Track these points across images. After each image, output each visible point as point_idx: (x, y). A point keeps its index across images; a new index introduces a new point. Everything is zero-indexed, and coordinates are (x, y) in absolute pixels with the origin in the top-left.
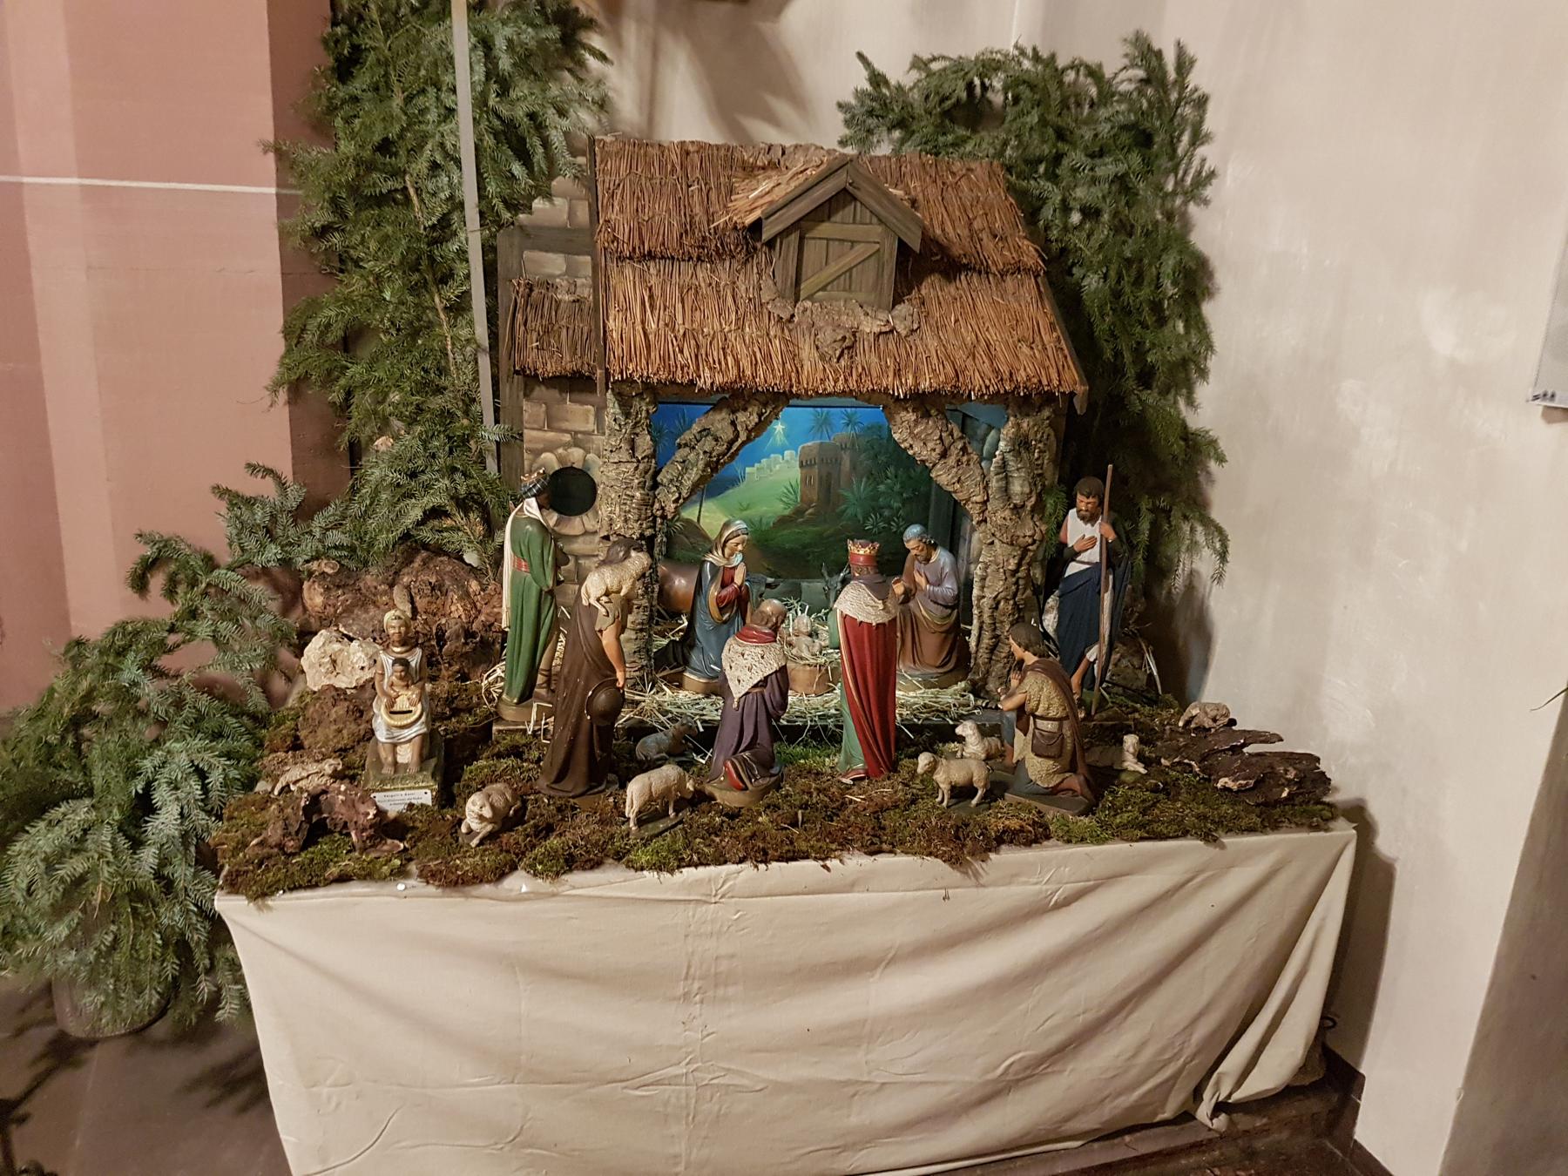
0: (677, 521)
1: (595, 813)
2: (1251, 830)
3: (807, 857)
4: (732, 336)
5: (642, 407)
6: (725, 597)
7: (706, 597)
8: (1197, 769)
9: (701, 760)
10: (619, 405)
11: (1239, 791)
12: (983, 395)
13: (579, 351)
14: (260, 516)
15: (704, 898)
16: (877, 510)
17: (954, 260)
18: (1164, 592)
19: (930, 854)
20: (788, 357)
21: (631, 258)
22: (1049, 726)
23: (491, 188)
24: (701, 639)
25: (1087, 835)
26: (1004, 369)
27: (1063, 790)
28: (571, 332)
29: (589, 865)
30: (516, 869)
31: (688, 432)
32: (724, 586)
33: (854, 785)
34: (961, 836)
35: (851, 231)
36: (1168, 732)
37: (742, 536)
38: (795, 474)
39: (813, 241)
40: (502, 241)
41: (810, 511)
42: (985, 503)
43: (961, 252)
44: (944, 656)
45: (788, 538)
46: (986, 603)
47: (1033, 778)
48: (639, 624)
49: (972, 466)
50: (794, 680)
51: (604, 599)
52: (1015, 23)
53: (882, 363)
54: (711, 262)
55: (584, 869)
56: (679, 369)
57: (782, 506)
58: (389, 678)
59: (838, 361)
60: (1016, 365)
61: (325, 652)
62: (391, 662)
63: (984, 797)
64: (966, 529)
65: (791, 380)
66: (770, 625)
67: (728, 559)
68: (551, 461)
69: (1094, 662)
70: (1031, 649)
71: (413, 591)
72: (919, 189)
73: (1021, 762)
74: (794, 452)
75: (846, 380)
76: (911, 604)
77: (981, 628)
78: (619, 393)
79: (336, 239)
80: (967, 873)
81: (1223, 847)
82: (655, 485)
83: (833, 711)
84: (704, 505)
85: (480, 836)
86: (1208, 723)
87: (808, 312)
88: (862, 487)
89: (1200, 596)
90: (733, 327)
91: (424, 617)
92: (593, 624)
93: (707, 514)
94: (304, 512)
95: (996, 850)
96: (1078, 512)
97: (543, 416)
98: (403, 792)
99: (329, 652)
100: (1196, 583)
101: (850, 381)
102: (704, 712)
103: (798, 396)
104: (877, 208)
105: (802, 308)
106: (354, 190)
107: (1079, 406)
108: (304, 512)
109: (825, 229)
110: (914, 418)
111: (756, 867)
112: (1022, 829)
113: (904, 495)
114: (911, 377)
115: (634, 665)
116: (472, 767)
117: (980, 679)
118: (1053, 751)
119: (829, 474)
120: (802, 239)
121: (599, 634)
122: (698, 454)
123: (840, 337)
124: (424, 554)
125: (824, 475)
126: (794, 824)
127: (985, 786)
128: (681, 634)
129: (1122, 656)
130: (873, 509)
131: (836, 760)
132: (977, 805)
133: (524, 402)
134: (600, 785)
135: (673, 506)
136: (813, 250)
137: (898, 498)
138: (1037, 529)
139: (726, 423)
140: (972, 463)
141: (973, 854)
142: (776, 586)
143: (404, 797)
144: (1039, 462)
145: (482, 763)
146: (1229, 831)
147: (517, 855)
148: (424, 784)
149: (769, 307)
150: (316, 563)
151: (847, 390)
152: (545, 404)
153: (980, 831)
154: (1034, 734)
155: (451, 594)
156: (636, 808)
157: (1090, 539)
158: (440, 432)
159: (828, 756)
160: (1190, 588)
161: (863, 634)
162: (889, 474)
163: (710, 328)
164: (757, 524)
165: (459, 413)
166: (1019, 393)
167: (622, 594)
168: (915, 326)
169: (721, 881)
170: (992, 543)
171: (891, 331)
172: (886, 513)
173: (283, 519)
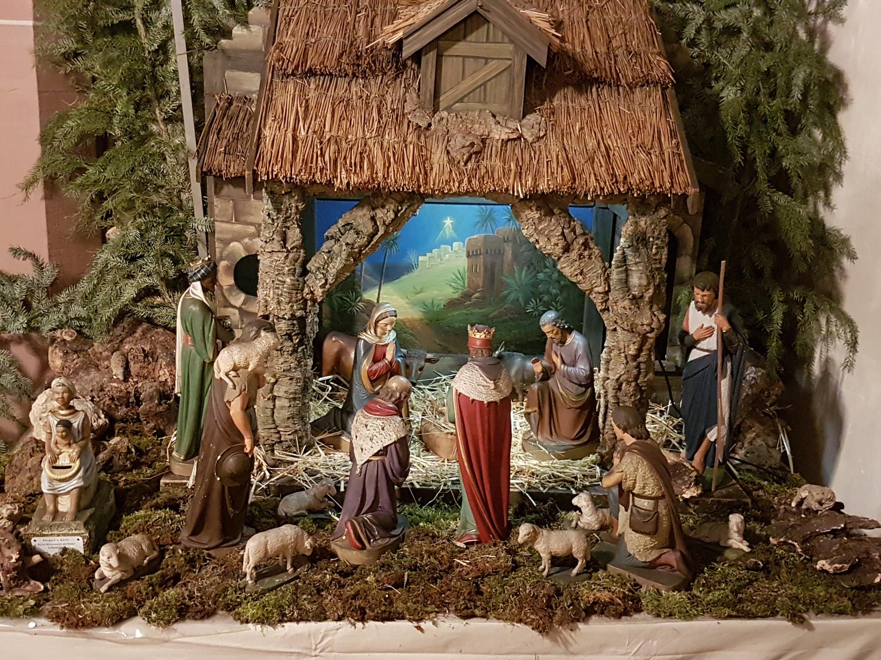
0: (359, 302)
1: (222, 565)
2: (841, 613)
3: (403, 618)
6: (376, 371)
7: (360, 373)
8: (800, 550)
10: (272, 202)
11: (835, 574)
14: (18, 291)
15: (304, 651)
17: (586, 74)
19: (520, 621)
21: (293, 74)
22: (645, 504)
23: (196, 18)
25: (676, 610)
27: (662, 565)
30: (136, 615)
31: (335, 226)
32: (375, 361)
35: (484, 49)
36: (782, 511)
37: (389, 318)
38: (463, 263)
39: (451, 58)
40: (208, 62)
41: (477, 295)
42: (607, 293)
43: (593, 67)
44: (578, 430)
47: (632, 553)
48: (292, 393)
50: (439, 447)
51: (232, 373)
54: (364, 77)
56: (319, 170)
61: (46, 408)
62: (56, 423)
66: (393, 399)
67: (380, 338)
70: (629, 431)
71: (130, 357)
72: (566, 12)
73: (621, 536)
74: (462, 243)
76: (550, 381)
77: (606, 407)
79: (79, 63)
80: (556, 641)
81: (811, 628)
82: (305, 272)
84: (382, 288)
85: (110, 583)
86: (815, 506)
87: (444, 121)
89: (834, 382)
92: (223, 395)
93: (385, 296)
94: (54, 288)
95: (585, 620)
96: (697, 302)
97: (231, 211)
98: (59, 538)
99: (49, 408)
103: (428, 196)
104: (507, 29)
105: (438, 118)
106: (92, 22)
108: (54, 288)
109: (461, 48)
110: (537, 216)
111: (354, 625)
112: (612, 602)
114: (530, 179)
115: (287, 429)
117: (607, 453)
118: (650, 528)
119: (493, 265)
120: (439, 57)
122: (341, 245)
123: (468, 143)
124: (145, 325)
125: (489, 267)
126: (398, 585)
127: (585, 557)
129: (758, 436)
130: (533, 293)
132: (578, 574)
133: (215, 199)
134: (235, 539)
135: (321, 290)
136: (449, 66)
137: (556, 285)
138: (655, 319)
140: (593, 257)
141: (561, 624)
143: (60, 542)
144: (657, 257)
145: (142, 512)
146: (820, 612)
148: (77, 532)
149: (409, 117)
150: (59, 331)
152: (233, 200)
153: (570, 601)
155: (160, 360)
156: (252, 564)
158: (159, 224)
160: (826, 373)
161: (475, 410)
162: (547, 264)
163: (356, 133)
164: (429, 305)
165: (175, 208)
167: (250, 370)
168: (542, 134)
169: (320, 636)
170: (615, 330)
171: (519, 138)
173: (39, 293)
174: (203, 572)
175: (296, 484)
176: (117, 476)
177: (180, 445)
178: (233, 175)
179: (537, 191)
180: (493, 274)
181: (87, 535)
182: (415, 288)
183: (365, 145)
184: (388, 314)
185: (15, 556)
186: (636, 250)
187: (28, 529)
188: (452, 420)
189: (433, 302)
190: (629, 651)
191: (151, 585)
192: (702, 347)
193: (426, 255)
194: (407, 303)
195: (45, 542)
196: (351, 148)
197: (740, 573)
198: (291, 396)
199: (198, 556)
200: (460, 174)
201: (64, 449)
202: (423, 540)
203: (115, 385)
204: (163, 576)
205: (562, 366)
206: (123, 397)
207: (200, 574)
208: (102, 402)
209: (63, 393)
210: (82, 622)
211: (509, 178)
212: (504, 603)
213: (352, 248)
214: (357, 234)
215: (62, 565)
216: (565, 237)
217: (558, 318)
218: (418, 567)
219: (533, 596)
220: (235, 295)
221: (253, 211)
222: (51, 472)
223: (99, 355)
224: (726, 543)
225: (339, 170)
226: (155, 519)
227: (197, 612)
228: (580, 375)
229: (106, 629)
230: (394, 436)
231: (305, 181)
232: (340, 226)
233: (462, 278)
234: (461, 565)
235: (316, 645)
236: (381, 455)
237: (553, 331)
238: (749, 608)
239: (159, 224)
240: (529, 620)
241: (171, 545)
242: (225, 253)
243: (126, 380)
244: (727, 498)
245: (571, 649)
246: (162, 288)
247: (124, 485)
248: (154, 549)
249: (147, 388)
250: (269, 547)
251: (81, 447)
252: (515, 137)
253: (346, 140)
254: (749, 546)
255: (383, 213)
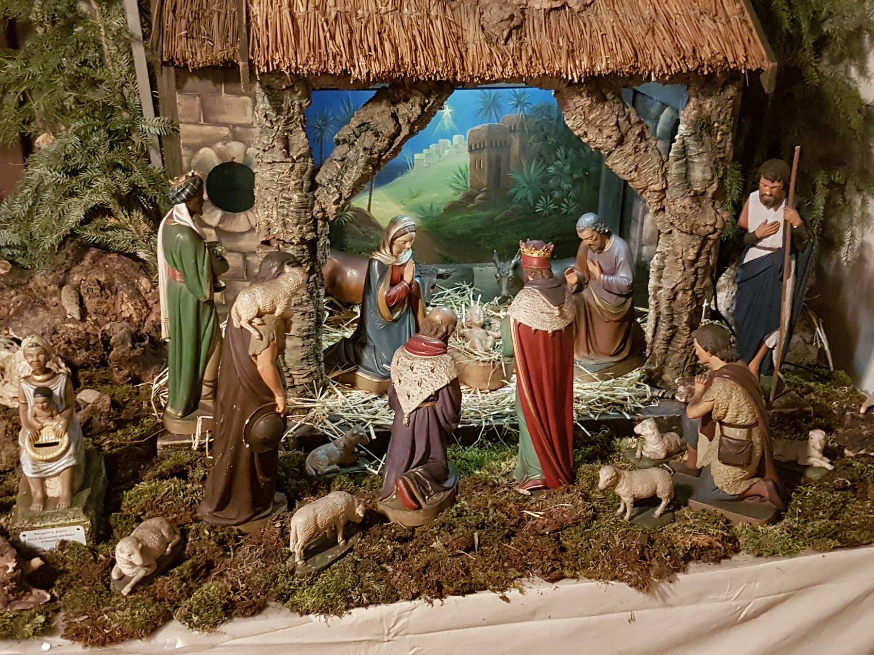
0: (347, 210)
1: (260, 544)
4: (388, 18)
5: (294, 101)
6: (395, 296)
9: (374, 471)
10: (269, 100)
12: (664, 75)
13: (230, 40)
15: (376, 638)
16: (547, 192)
18: (833, 263)
19: (615, 578)
20: (450, 40)
22: (738, 434)
24: (371, 336)
25: (778, 548)
26: (686, 45)
28: (222, 17)
29: (249, 611)
30: (171, 618)
32: (393, 284)
33: (532, 495)
34: (647, 556)
36: (849, 418)
37: (409, 234)
38: (464, 159)
42: (663, 191)
44: (617, 346)
45: (459, 223)
46: (664, 294)
47: (719, 486)
48: (305, 331)
49: (650, 152)
50: (468, 376)
51: (257, 321)
52: (232, 435)
53: (555, 43)
55: (244, 615)
56: (331, 58)
57: (453, 192)
58: (32, 408)
59: (506, 44)
60: (700, 41)
62: (32, 391)
63: (668, 506)
64: (638, 210)
65: (454, 67)
66: (439, 335)
67: (397, 257)
68: (210, 157)
69: (773, 349)
71: (83, 291)
74: (463, 136)
75: (515, 65)
76: (585, 293)
77: (657, 319)
78: (268, 87)
82: (314, 186)
83: (508, 410)
84: (374, 193)
85: (132, 583)
88: (532, 171)
90: (390, 8)
91: (94, 318)
93: (377, 203)
95: (684, 570)
96: (762, 196)
97: (197, 109)
98: (54, 530)
100: (867, 256)
101: (519, 63)
102: (377, 417)
107: (767, 83)
110: (588, 103)
112: (711, 547)
113: (575, 176)
114: (585, 58)
116: (132, 492)
117: (656, 369)
119: (498, 160)
121: (253, 359)
122: (358, 151)
123: (507, 16)
124: (94, 251)
125: (494, 161)
126: (470, 549)
127: (669, 496)
128: (356, 325)
130: (543, 190)
131: (512, 465)
132: (661, 515)
133: (178, 96)
134: (266, 509)
135: (334, 207)
137: (569, 180)
139: (387, 116)
140: (650, 149)
141: (660, 576)
142: (448, 276)
144: (722, 145)
145: (143, 486)
147: (172, 603)
148: (75, 521)
151: (516, 75)
152: (199, 96)
154: (721, 441)
155: (120, 293)
156: (301, 542)
157: (773, 224)
158: (99, 127)
159: (504, 459)
161: (538, 342)
166: (702, 72)
167: (276, 314)
170: (671, 232)
171: (563, 7)
172: (557, 195)
174: (240, 554)
175: (318, 434)
176: (98, 438)
177: (174, 398)
178: (201, 65)
179: (594, 73)
180: (498, 170)
181: (89, 522)
182: (410, 191)
183: (382, 22)
184: (406, 229)
185: (12, 565)
186: (699, 138)
187: (14, 522)
188: (509, 353)
189: (431, 207)
190: (730, 596)
191: (184, 580)
192: (764, 246)
193: (422, 152)
194: (403, 210)
195: (38, 537)
196: (366, 27)
197: (834, 497)
198: (305, 334)
199: (228, 535)
200: (502, 56)
201: (47, 422)
202: (482, 490)
203: (70, 325)
204: (194, 566)
205: (602, 276)
206: (83, 340)
207: (237, 558)
208: (56, 346)
209: (38, 355)
210: (110, 638)
211: (560, 58)
212: (594, 560)
213: (371, 154)
214: (376, 136)
215: (65, 564)
216: (619, 127)
217: (598, 222)
218: (486, 524)
219: (625, 549)
220: (211, 212)
221: (226, 108)
222: (35, 451)
223: (44, 291)
224: (806, 462)
225: (355, 57)
226: (163, 493)
227: (247, 608)
228: (622, 285)
229: (139, 641)
230: (446, 379)
231: (314, 72)
232: (353, 126)
233: (464, 177)
234: (533, 517)
235: (389, 630)
236: (431, 400)
237: (592, 236)
238: (852, 536)
239: (99, 127)
240: (627, 577)
241: (191, 524)
242: (194, 162)
243: (83, 319)
244: (787, 408)
245: (668, 601)
246: (114, 207)
247: (110, 450)
248: (175, 532)
249: (117, 331)
250: (319, 522)
251: (67, 418)
252: (559, 5)
253: (356, 16)
254: (831, 463)
255: (407, 109)
